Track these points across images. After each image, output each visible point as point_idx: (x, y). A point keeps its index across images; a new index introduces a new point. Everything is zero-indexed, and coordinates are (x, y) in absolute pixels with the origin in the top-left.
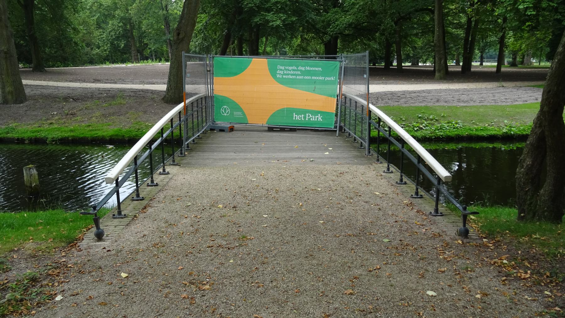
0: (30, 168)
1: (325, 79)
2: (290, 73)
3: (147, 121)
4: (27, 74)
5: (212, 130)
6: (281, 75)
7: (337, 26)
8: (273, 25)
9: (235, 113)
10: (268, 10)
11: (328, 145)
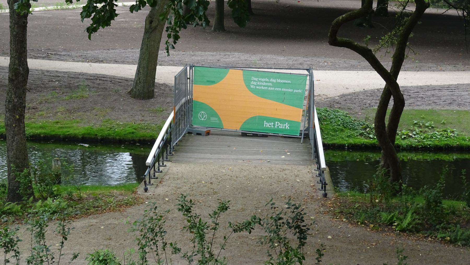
3: (117, 119)
5: (189, 133)
11: (289, 150)
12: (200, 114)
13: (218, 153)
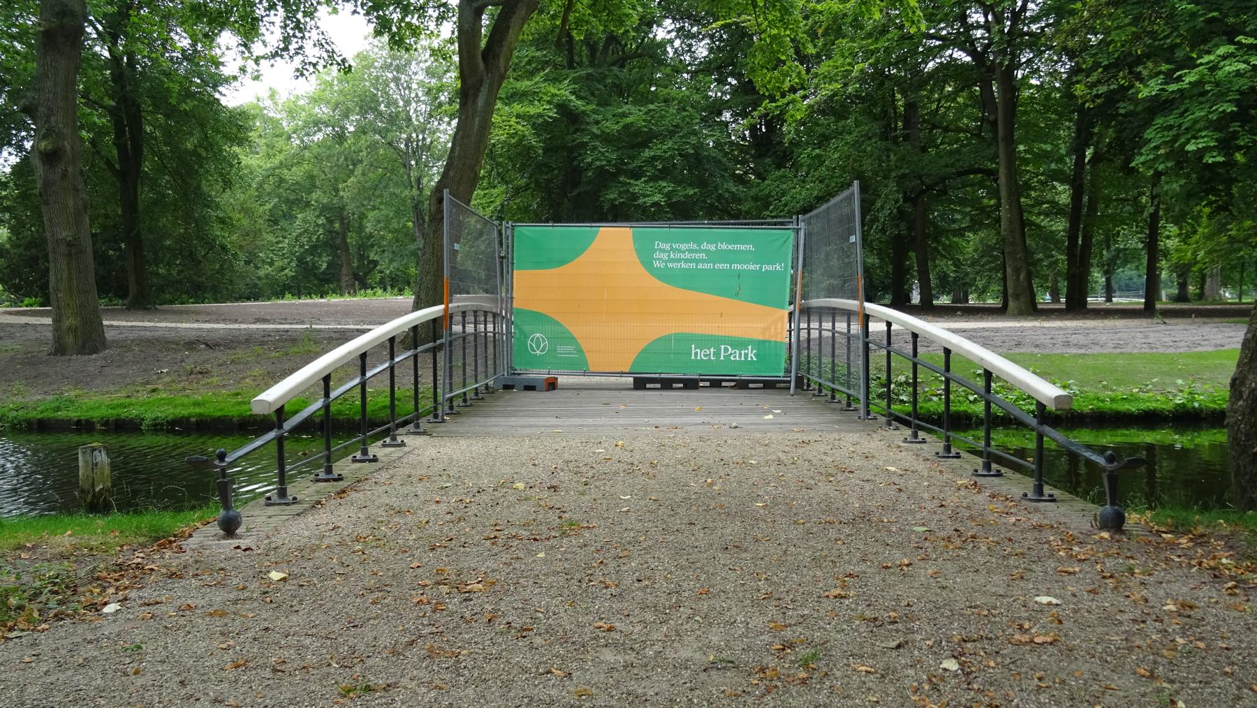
0: (94, 449)
1: (761, 268)
2: (683, 256)
4: (114, 313)
5: (508, 387)
6: (663, 261)
7: (785, 205)
8: (645, 203)
9: (560, 349)
10: (636, 175)
12: (532, 341)
13: (580, 416)
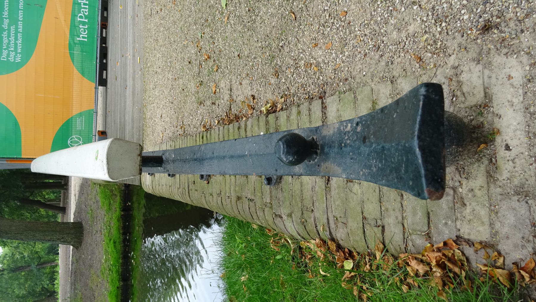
3: (101, 261)
